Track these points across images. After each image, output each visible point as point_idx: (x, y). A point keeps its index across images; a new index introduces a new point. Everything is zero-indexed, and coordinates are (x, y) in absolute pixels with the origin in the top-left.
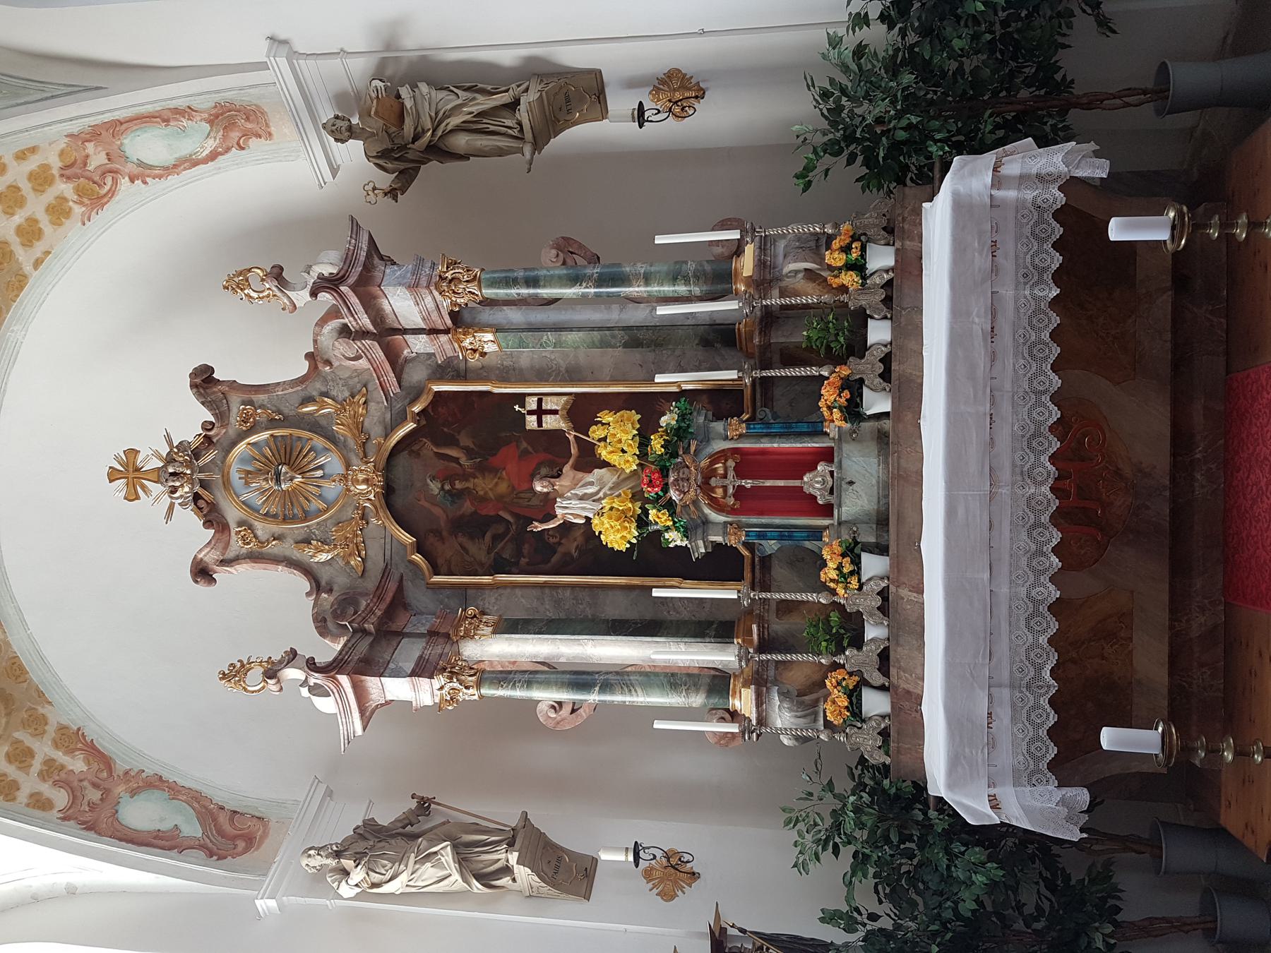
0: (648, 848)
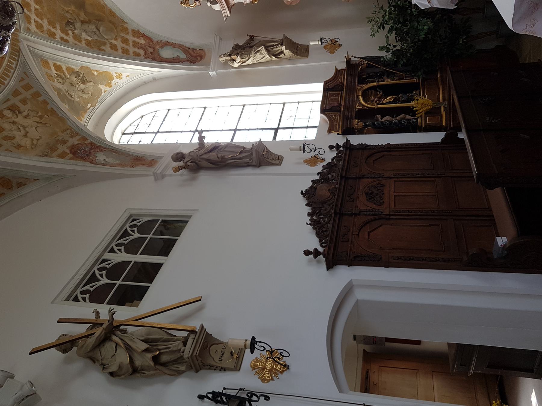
0: (325, 39)
